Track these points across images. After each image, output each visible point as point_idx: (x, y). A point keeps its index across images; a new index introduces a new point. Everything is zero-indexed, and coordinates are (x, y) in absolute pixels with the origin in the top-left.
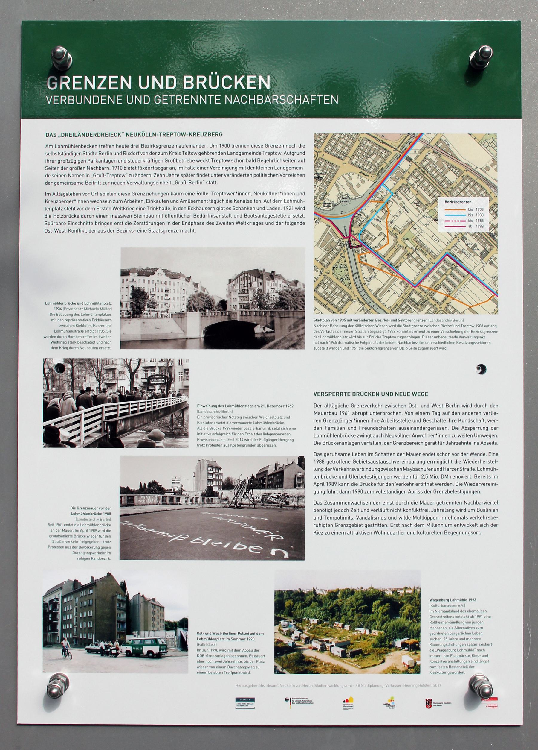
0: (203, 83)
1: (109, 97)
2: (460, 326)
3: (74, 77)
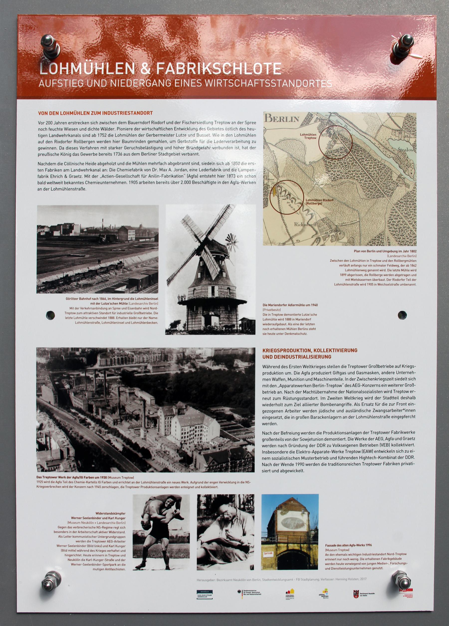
0: (193, 69)
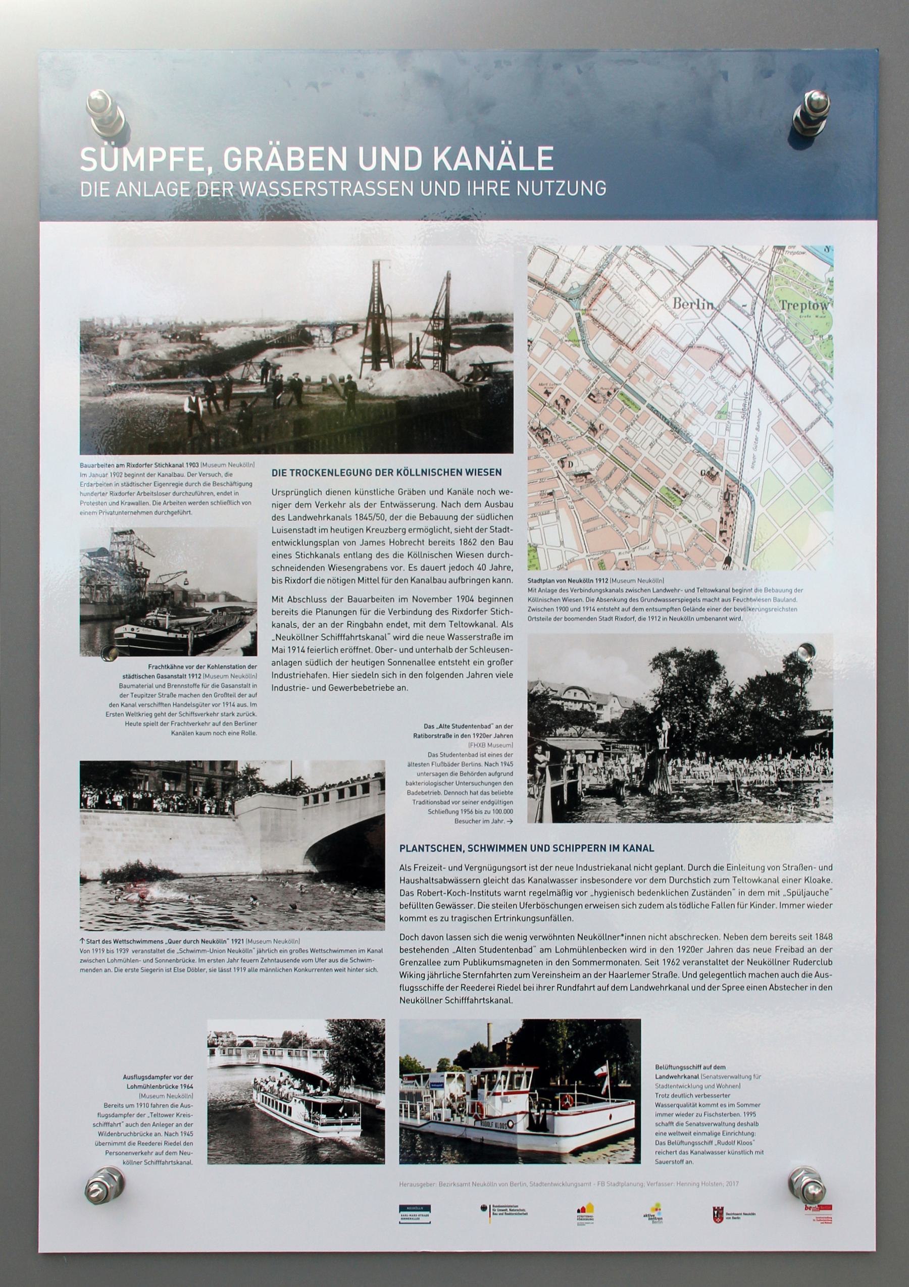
0: (256, 160)
1: (403, 183)
2: (696, 590)
3: (311, 149)
